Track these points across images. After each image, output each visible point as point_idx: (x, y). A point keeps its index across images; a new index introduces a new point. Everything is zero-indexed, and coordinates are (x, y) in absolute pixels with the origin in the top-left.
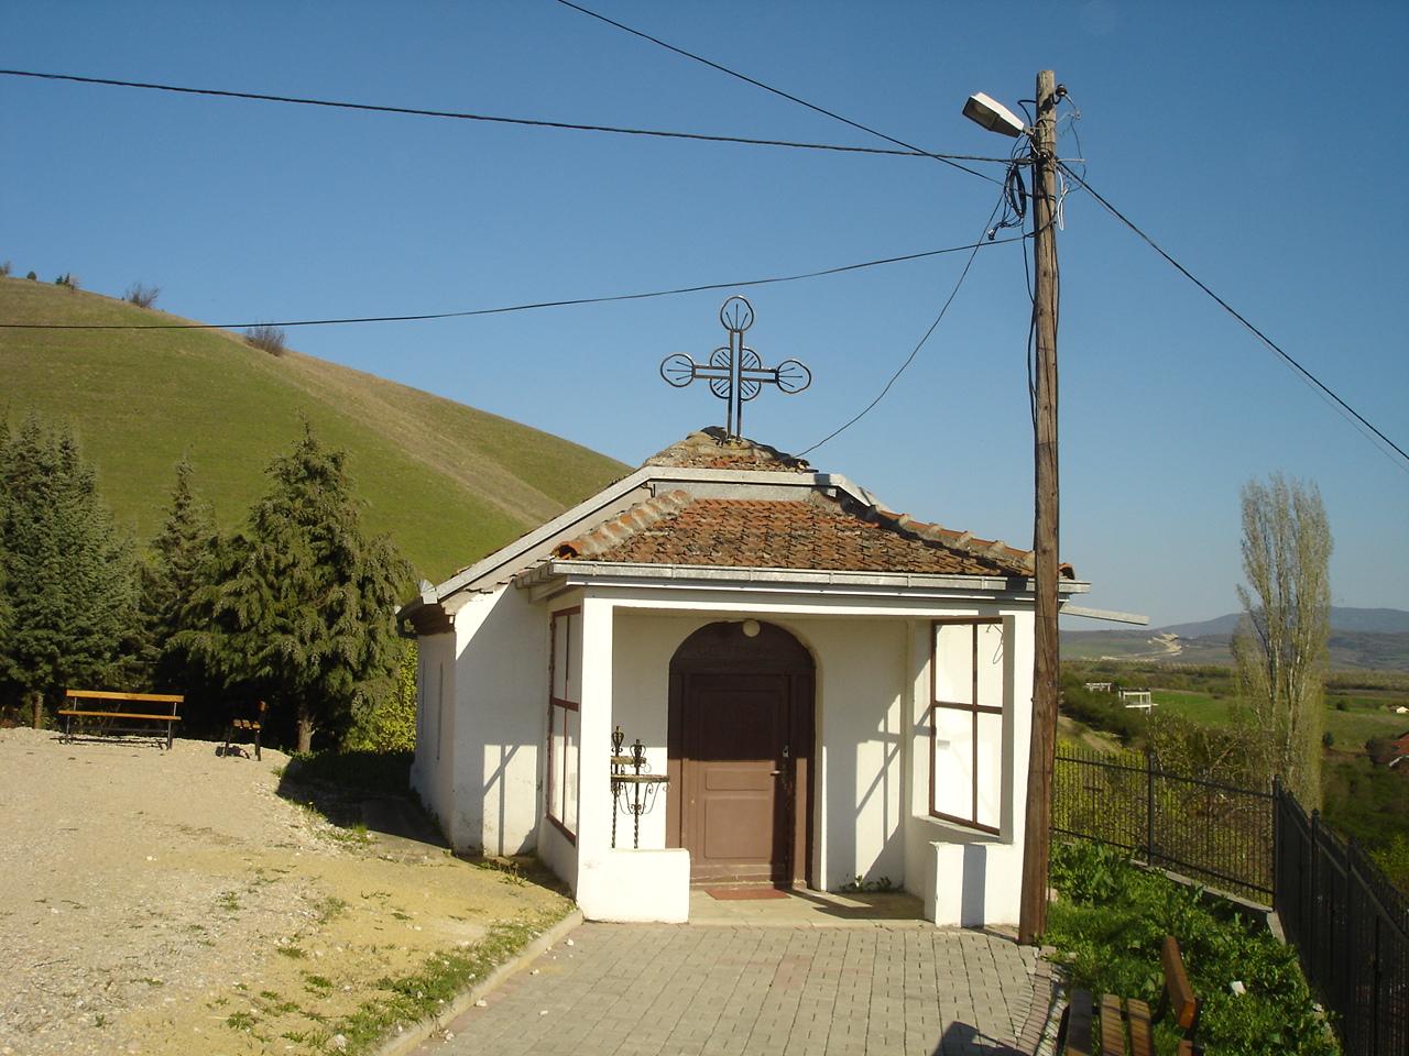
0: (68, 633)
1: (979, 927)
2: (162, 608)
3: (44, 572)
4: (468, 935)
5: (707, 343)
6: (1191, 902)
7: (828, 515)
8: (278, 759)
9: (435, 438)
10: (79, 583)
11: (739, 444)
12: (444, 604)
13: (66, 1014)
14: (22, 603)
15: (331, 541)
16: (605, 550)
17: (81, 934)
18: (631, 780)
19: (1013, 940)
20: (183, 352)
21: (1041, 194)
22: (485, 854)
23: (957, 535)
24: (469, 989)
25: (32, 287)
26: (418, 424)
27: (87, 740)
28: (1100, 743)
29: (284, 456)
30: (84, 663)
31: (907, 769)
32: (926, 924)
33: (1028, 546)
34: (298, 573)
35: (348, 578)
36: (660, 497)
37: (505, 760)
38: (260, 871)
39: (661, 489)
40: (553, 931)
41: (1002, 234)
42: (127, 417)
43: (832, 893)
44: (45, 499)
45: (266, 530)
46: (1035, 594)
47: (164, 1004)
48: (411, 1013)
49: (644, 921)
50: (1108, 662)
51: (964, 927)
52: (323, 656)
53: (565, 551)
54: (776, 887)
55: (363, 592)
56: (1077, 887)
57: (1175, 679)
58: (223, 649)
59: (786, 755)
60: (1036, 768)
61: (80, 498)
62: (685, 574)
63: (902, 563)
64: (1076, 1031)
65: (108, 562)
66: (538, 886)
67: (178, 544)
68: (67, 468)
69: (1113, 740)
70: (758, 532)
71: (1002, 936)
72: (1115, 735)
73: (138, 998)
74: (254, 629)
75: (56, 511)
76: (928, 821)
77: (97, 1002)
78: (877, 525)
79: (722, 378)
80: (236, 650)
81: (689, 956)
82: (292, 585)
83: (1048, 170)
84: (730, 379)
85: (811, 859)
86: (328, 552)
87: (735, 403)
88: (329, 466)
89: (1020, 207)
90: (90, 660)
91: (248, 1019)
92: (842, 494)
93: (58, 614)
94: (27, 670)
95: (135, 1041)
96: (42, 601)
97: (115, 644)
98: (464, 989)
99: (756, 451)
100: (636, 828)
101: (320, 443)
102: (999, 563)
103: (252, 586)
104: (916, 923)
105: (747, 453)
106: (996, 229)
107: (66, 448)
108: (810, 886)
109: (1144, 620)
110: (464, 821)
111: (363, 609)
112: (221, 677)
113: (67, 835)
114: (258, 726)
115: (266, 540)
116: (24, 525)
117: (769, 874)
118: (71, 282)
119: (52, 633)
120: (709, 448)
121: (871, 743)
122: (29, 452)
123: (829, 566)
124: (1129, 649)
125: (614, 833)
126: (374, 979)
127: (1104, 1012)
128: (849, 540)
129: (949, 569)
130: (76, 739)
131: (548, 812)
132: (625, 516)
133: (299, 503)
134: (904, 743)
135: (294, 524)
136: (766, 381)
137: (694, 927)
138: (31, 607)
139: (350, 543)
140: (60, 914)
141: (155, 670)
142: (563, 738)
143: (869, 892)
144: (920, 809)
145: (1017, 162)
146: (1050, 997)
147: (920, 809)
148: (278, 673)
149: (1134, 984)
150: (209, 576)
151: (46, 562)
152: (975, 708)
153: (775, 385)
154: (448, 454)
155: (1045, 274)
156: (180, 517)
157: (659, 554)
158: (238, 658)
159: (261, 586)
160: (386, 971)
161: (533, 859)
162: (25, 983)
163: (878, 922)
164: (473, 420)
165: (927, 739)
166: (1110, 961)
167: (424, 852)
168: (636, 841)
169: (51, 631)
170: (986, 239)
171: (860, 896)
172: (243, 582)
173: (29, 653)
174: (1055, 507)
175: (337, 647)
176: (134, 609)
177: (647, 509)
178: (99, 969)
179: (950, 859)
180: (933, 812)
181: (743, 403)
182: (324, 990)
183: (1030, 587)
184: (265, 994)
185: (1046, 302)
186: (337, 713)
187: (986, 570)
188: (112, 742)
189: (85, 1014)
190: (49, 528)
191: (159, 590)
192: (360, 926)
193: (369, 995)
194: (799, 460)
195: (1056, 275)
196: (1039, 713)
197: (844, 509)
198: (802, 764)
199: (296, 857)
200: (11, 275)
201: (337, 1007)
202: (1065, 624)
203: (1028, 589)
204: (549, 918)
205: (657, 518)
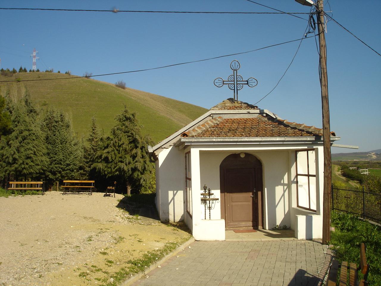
0: (64, 165)
1: (311, 239)
2: (90, 157)
3: (57, 149)
4: (159, 246)
5: (227, 74)
6: (374, 231)
7: (263, 121)
8: (121, 197)
9: (167, 109)
10: (66, 152)
11: (237, 103)
12: (155, 152)
13: (31, 274)
14: (52, 158)
15: (133, 137)
16: (196, 134)
17: (44, 250)
18: (208, 200)
19: (321, 243)
20: (99, 90)
21: (320, 22)
22: (170, 222)
23: (300, 125)
24: (156, 263)
25: (59, 75)
26: (162, 105)
27: (70, 194)
28: (354, 184)
29: (119, 115)
30: (69, 173)
31: (290, 192)
32: (296, 239)
33: (321, 127)
34: (124, 146)
35: (138, 147)
36: (214, 119)
37: (174, 195)
38: (102, 229)
39: (215, 116)
40: (185, 244)
41: (309, 35)
42: (85, 107)
43: (270, 230)
44: (56, 130)
45: (115, 135)
46: (323, 141)
47: (61, 270)
48: (136, 271)
49: (212, 240)
50: (356, 161)
51: (307, 239)
52: (132, 168)
53: (184, 135)
54: (254, 229)
55: (142, 150)
56: (342, 226)
57: (375, 165)
58: (106, 168)
59: (255, 191)
60: (326, 192)
61: (66, 129)
62: (219, 140)
63: (284, 134)
64: (334, 273)
65: (74, 146)
66: (183, 231)
67: (93, 140)
68: (62, 121)
69: (358, 183)
70: (242, 127)
71: (317, 242)
72: (358, 182)
73: (54, 269)
74: (113, 162)
75: (59, 133)
76: (296, 209)
77: (41, 270)
78: (277, 123)
79: (232, 84)
80: (109, 168)
81: (223, 250)
82: (123, 149)
83: (321, 15)
84: (234, 84)
85: (263, 221)
86: (132, 140)
87: (236, 90)
88: (131, 117)
89: (314, 27)
90: (70, 172)
91: (85, 274)
92: (267, 115)
93: (61, 160)
94: (54, 175)
95: (50, 282)
96: (57, 157)
97: (77, 168)
98: (154, 263)
99: (242, 104)
100: (210, 213)
101: (129, 111)
102: (313, 133)
103: (112, 150)
104: (292, 239)
105: (240, 105)
106: (307, 34)
107: (61, 116)
108: (263, 228)
109: (357, 147)
110: (164, 213)
111: (142, 155)
112: (105, 175)
113: (52, 221)
114: (114, 188)
115: (115, 138)
116: (51, 137)
117: (252, 225)
118: (69, 73)
119: (60, 165)
120: (229, 104)
121: (279, 186)
122: (51, 117)
123: (262, 136)
124: (362, 157)
125: (205, 215)
126: (127, 261)
127: (342, 267)
128: (268, 128)
129: (297, 135)
130: (66, 194)
131: (187, 209)
132: (203, 125)
133: (124, 127)
134: (289, 186)
135: (123, 133)
136: (245, 84)
137: (227, 242)
138: (54, 159)
139: (137, 137)
140: (40, 244)
141: (89, 174)
142: (296, 185)
143: (280, 229)
144: (294, 205)
145: (312, 14)
146: (330, 261)
147: (294, 205)
148: (120, 174)
149: (355, 256)
150: (101, 148)
151: (57, 146)
152: (308, 176)
153: (247, 85)
154: (170, 113)
155: (322, 46)
156: (94, 133)
157: (212, 134)
158: (109, 170)
159: (114, 150)
160: (131, 258)
161: (183, 223)
162: (22, 266)
163: (281, 239)
164: (177, 104)
165: (295, 185)
166: (349, 249)
167: (153, 222)
168: (210, 217)
169: (59, 165)
170: (304, 37)
171: (278, 231)
172: (110, 149)
173: (54, 171)
174: (328, 115)
175: (136, 166)
176: (82, 158)
177: (210, 122)
178: (45, 260)
179: (302, 220)
180: (298, 206)
181: (238, 91)
182: (110, 264)
183: (322, 139)
184: (93, 266)
185: (323, 54)
186: (137, 184)
187: (309, 135)
188: (76, 194)
189: (36, 274)
190: (58, 137)
191: (89, 153)
192: (126, 246)
193: (124, 265)
194: (255, 106)
195: (325, 46)
196: (326, 176)
197: (268, 119)
198: (259, 193)
199: (114, 225)
200: (54, 72)
201: (113, 270)
202: (334, 150)
203: (321, 140)
204: (184, 240)
205: (213, 124)
